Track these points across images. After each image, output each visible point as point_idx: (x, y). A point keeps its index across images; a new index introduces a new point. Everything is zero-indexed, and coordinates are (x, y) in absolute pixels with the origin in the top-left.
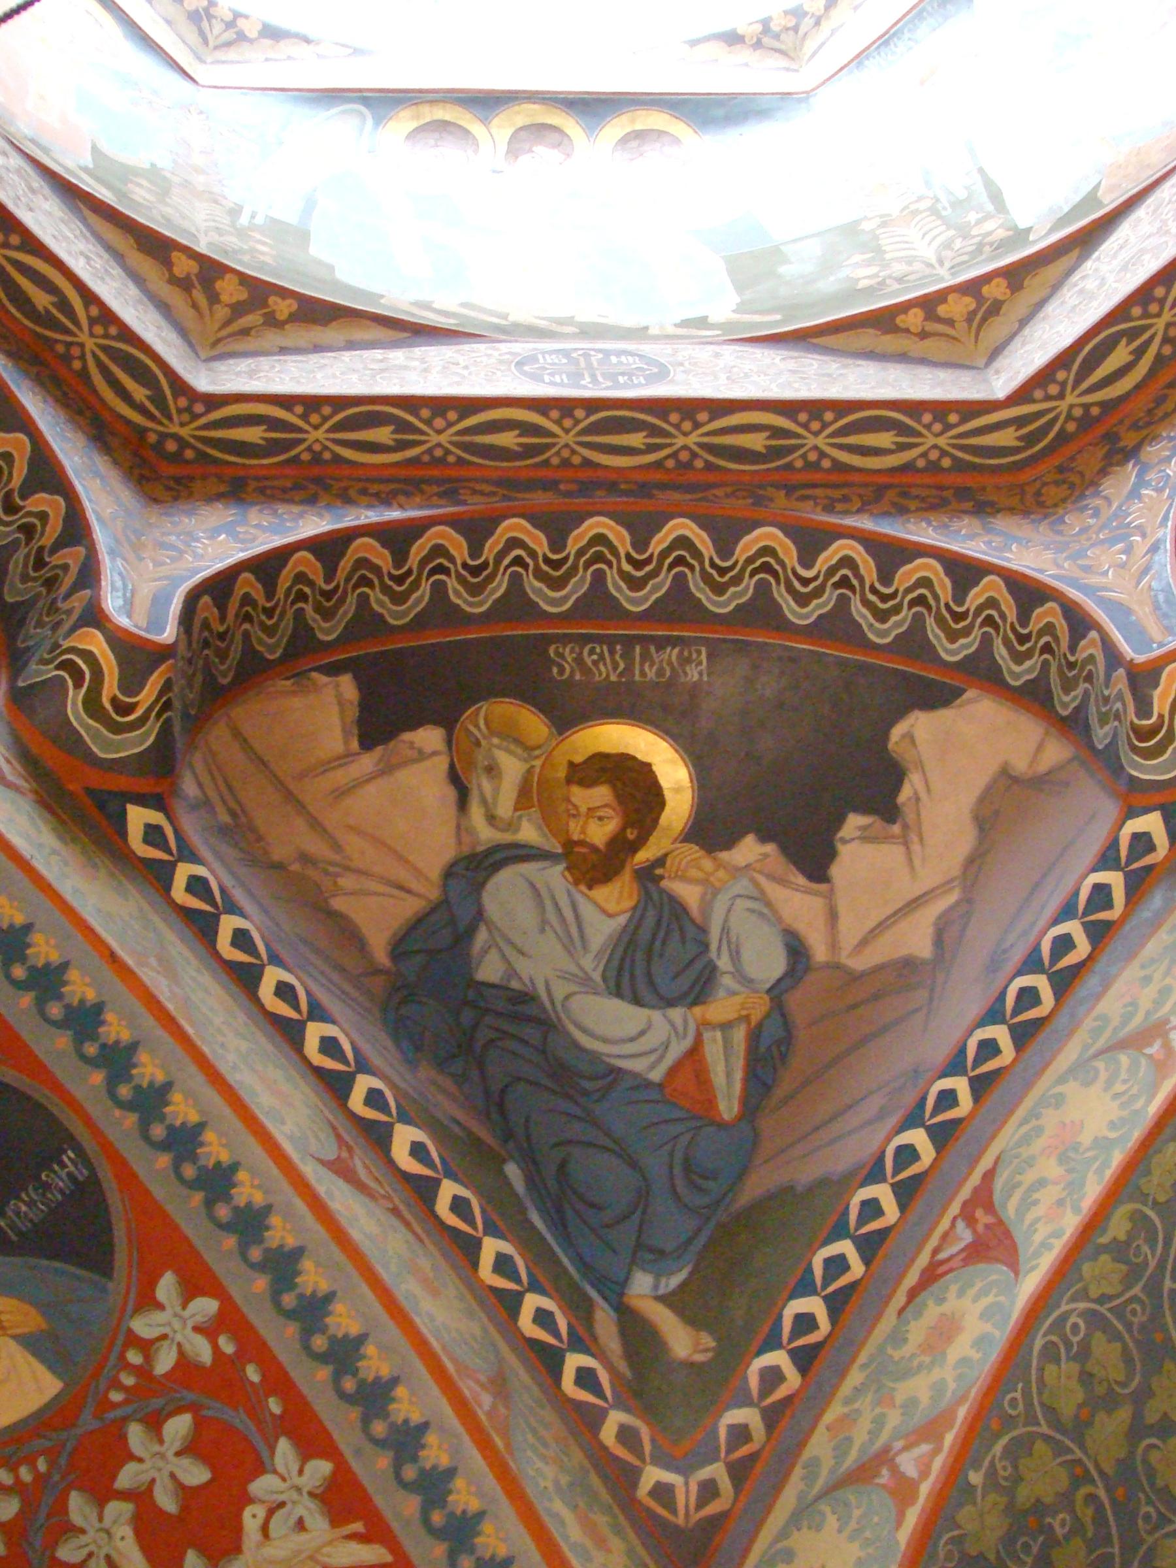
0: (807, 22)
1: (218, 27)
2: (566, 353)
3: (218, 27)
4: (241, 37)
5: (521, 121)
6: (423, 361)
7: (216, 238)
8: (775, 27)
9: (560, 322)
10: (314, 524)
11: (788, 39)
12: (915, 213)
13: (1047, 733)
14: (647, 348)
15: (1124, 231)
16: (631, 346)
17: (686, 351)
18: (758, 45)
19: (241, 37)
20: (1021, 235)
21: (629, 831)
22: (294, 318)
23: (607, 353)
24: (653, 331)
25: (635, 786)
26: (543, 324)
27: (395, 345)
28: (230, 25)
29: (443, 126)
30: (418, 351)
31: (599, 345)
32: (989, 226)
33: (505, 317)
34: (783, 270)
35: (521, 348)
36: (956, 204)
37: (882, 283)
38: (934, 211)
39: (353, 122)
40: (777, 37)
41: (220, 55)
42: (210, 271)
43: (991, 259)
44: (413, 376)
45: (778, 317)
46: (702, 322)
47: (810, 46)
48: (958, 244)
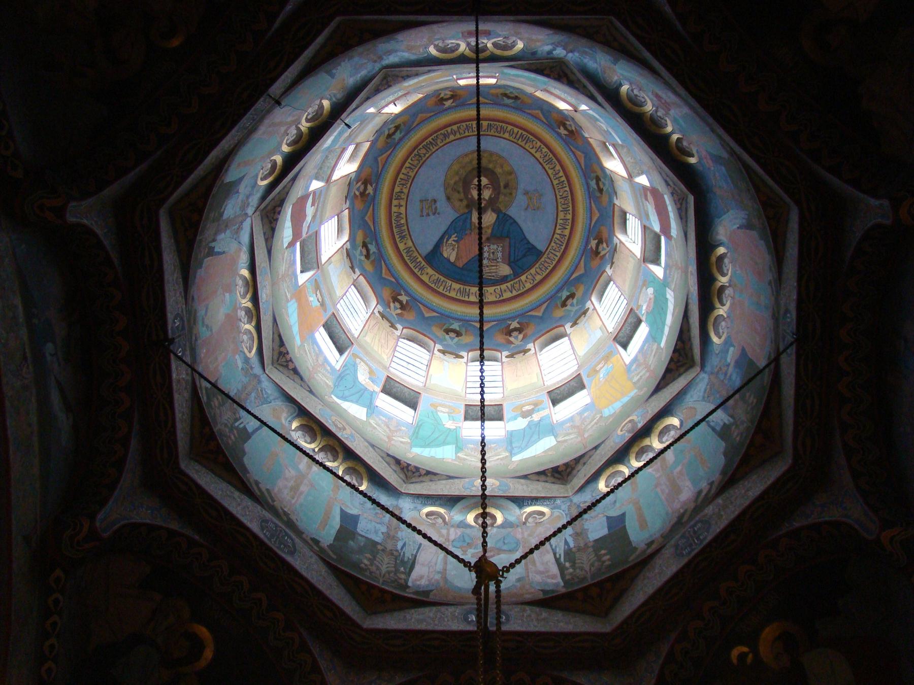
0: (417, 474)
1: (284, 360)
2: (277, 526)
3: (284, 360)
4: (287, 366)
5: (331, 443)
6: (242, 500)
9: (285, 513)
10: (174, 526)
11: (410, 474)
12: (392, 554)
13: (445, 579)
14: (297, 540)
15: (426, 610)
17: (306, 550)
18: (402, 469)
19: (287, 366)
20: (405, 587)
21: (494, 216)
23: (287, 534)
24: (304, 536)
25: (198, 645)
27: (238, 489)
28: (287, 361)
30: (243, 496)
31: (287, 530)
35: (267, 515)
36: (402, 561)
37: (366, 570)
38: (396, 559)
40: (408, 471)
42: (212, 437)
43: (395, 588)
45: (335, 557)
47: (414, 480)
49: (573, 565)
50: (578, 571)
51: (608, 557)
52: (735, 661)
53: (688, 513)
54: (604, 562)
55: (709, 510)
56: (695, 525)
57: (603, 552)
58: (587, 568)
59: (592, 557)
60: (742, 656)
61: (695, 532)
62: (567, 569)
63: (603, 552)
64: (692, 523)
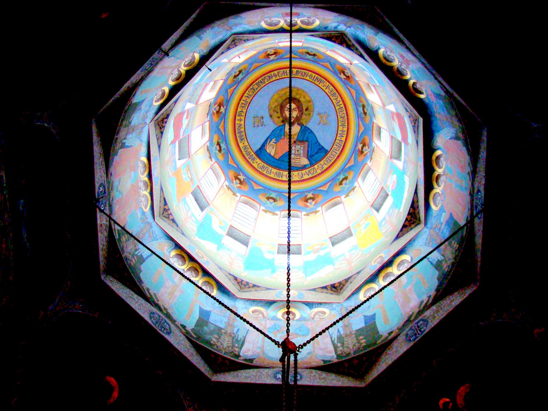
0: (247, 286)
1: (167, 213)
2: (160, 316)
3: (167, 213)
4: (168, 218)
6: (138, 300)
7: (128, 255)
8: (243, 282)
9: (165, 309)
11: (243, 286)
12: (231, 336)
14: (172, 326)
16: (170, 323)
17: (177, 332)
18: (238, 283)
19: (168, 218)
22: (333, 37)
23: (165, 321)
24: (176, 323)
26: (162, 307)
28: (168, 215)
29: (183, 257)
31: (166, 319)
32: (237, 349)
33: (158, 301)
34: (205, 328)
35: (154, 309)
36: (237, 340)
39: (171, 245)
40: (242, 284)
41: (163, 218)
44: (134, 302)
45: (195, 337)
46: (184, 327)
47: (245, 290)
48: (230, 348)
49: (343, 345)
50: (345, 349)
51: (364, 340)
52: (441, 407)
53: (414, 315)
54: (361, 344)
55: (427, 313)
56: (419, 322)
57: (361, 337)
58: (351, 348)
59: (355, 341)
60: (446, 404)
61: (418, 327)
62: (339, 347)
63: (361, 337)
64: (417, 321)
